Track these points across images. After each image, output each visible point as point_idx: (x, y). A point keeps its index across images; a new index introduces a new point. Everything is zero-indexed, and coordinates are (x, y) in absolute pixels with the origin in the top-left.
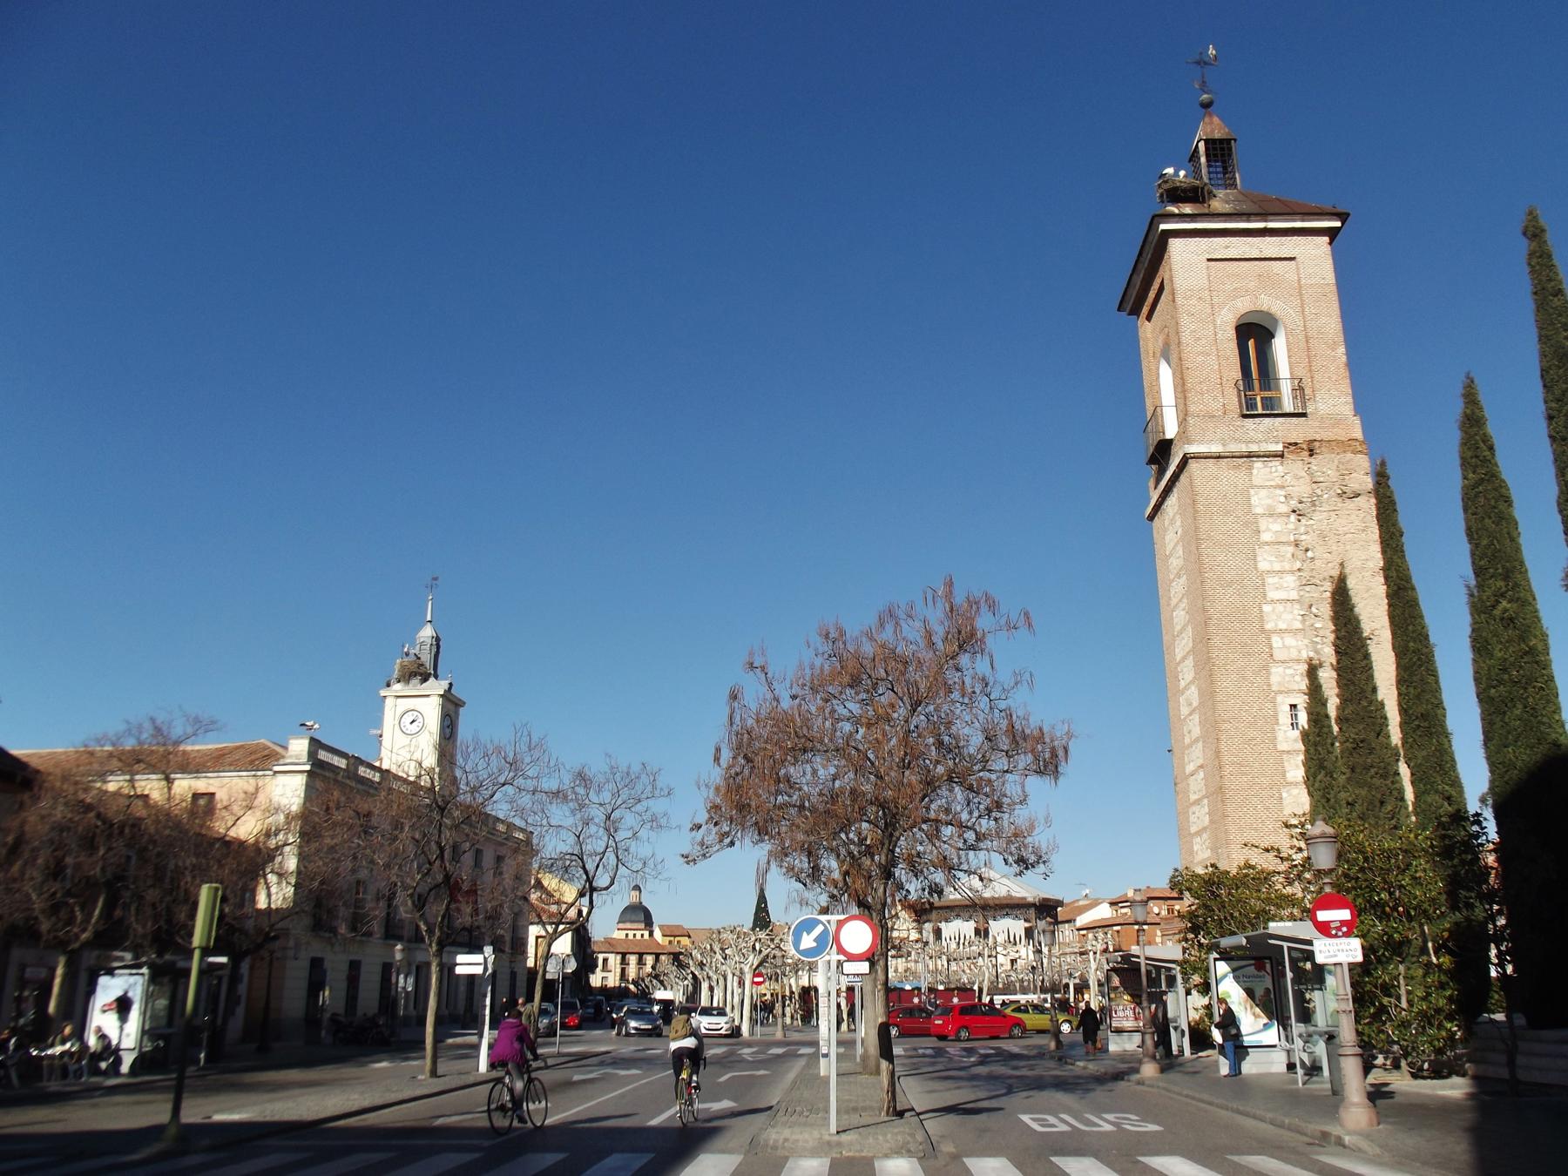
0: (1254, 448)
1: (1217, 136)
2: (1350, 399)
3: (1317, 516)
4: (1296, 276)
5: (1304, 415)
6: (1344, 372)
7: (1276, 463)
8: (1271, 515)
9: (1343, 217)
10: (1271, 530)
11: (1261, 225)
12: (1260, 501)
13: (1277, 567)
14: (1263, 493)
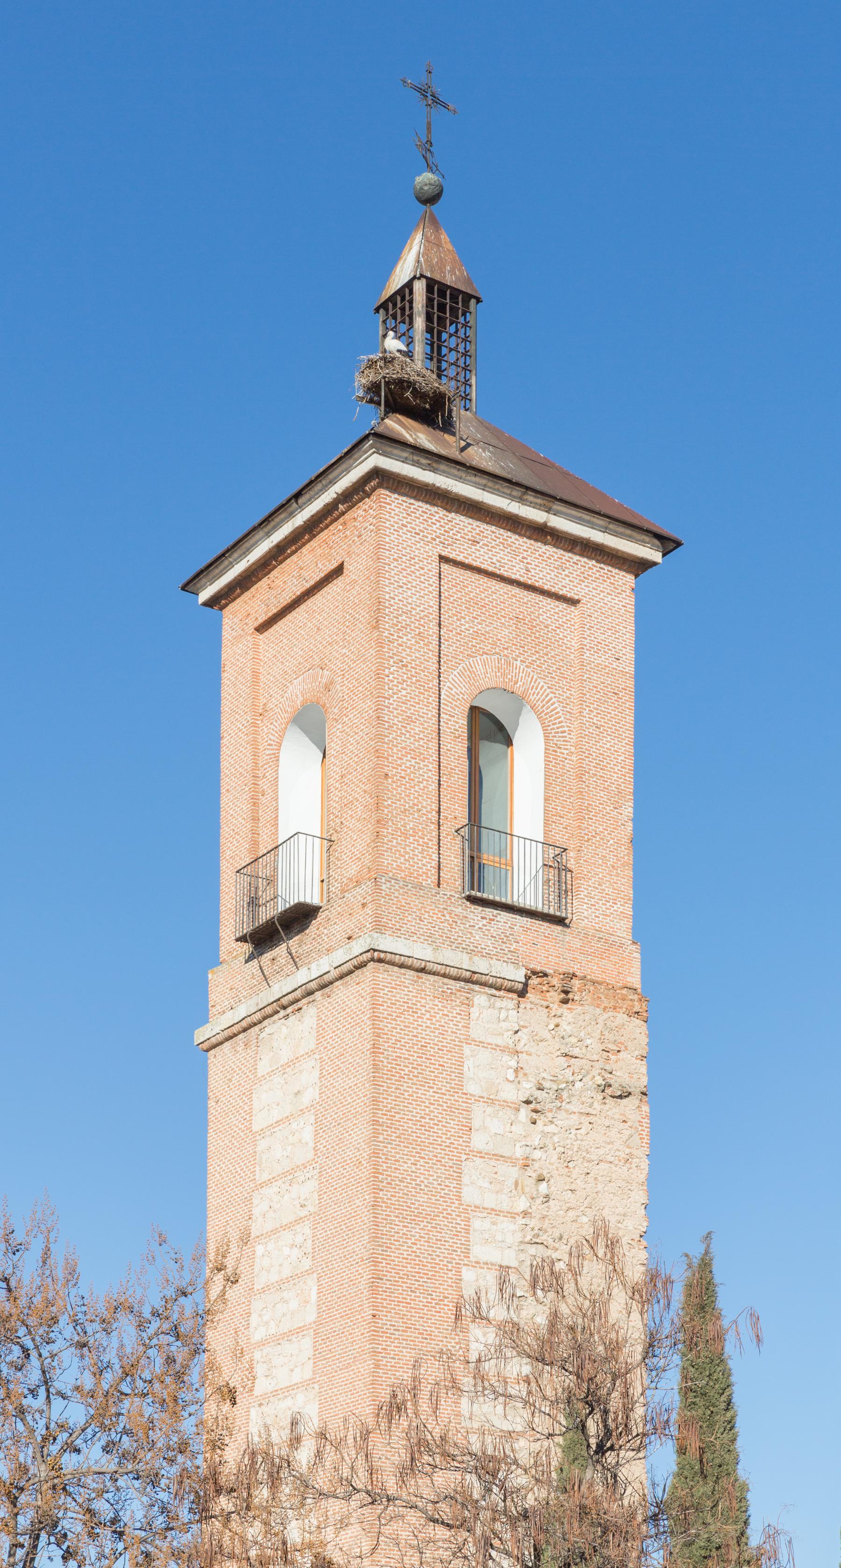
0: (481, 966)
1: (449, 279)
2: (629, 910)
3: (562, 1119)
4: (576, 639)
5: (560, 921)
6: (625, 854)
7: (509, 1002)
8: (491, 1102)
9: (668, 544)
10: (492, 1129)
11: (537, 515)
12: (480, 1070)
13: (490, 1203)
14: (484, 1055)
